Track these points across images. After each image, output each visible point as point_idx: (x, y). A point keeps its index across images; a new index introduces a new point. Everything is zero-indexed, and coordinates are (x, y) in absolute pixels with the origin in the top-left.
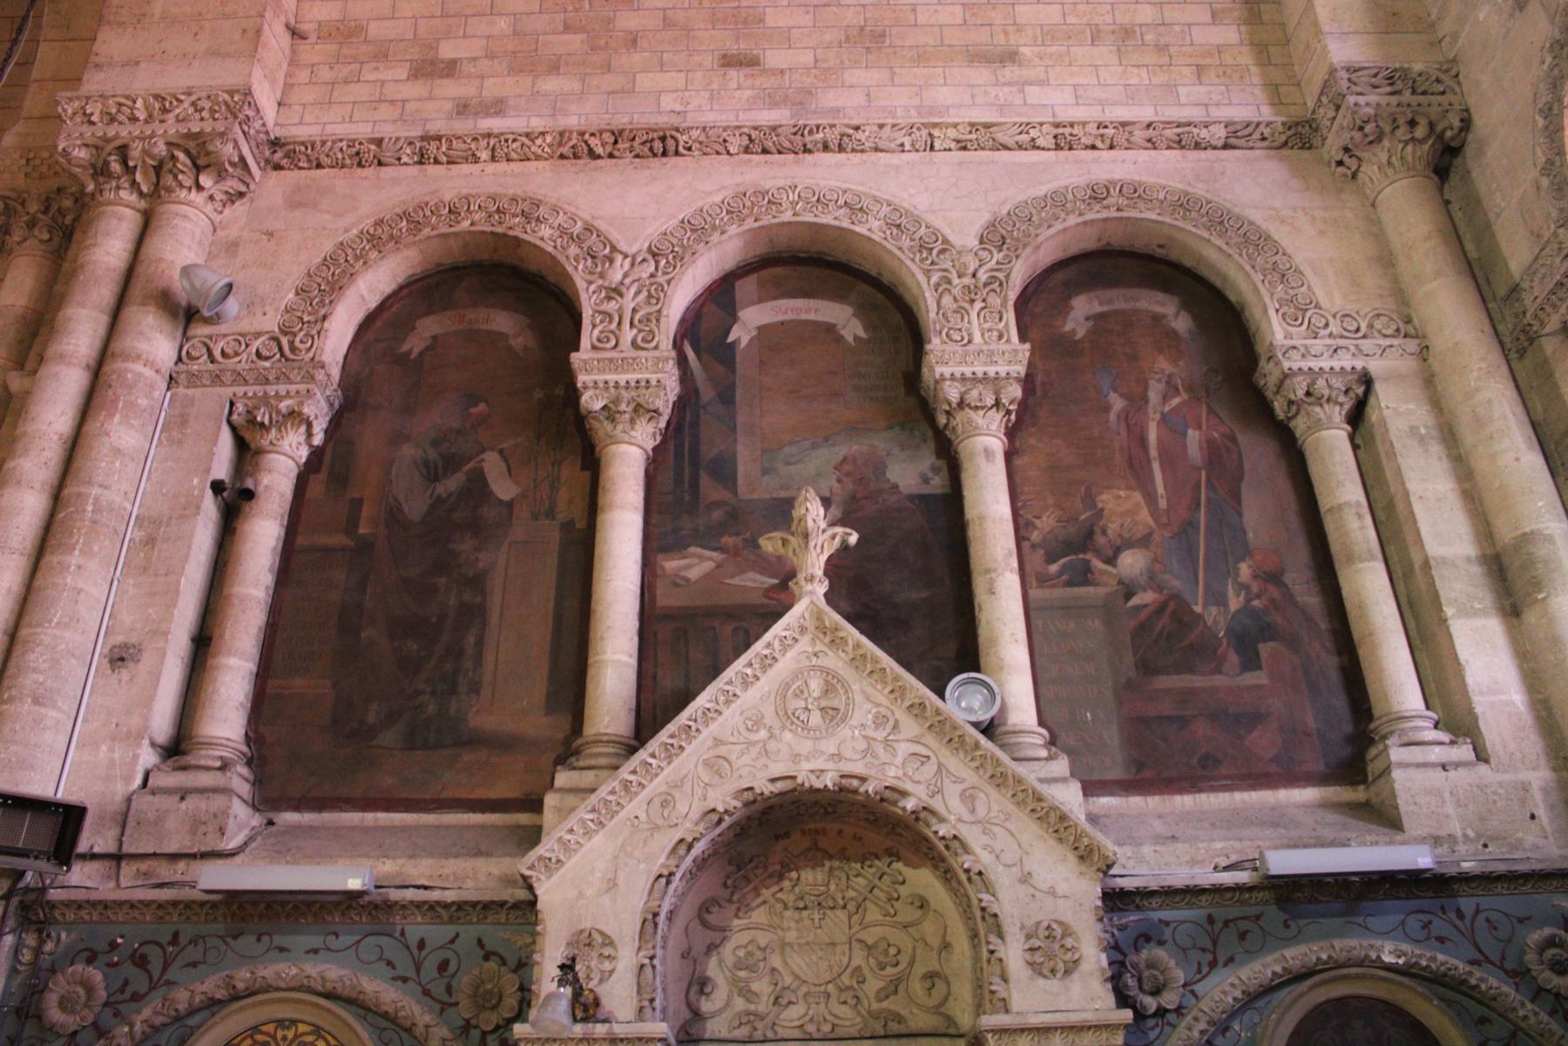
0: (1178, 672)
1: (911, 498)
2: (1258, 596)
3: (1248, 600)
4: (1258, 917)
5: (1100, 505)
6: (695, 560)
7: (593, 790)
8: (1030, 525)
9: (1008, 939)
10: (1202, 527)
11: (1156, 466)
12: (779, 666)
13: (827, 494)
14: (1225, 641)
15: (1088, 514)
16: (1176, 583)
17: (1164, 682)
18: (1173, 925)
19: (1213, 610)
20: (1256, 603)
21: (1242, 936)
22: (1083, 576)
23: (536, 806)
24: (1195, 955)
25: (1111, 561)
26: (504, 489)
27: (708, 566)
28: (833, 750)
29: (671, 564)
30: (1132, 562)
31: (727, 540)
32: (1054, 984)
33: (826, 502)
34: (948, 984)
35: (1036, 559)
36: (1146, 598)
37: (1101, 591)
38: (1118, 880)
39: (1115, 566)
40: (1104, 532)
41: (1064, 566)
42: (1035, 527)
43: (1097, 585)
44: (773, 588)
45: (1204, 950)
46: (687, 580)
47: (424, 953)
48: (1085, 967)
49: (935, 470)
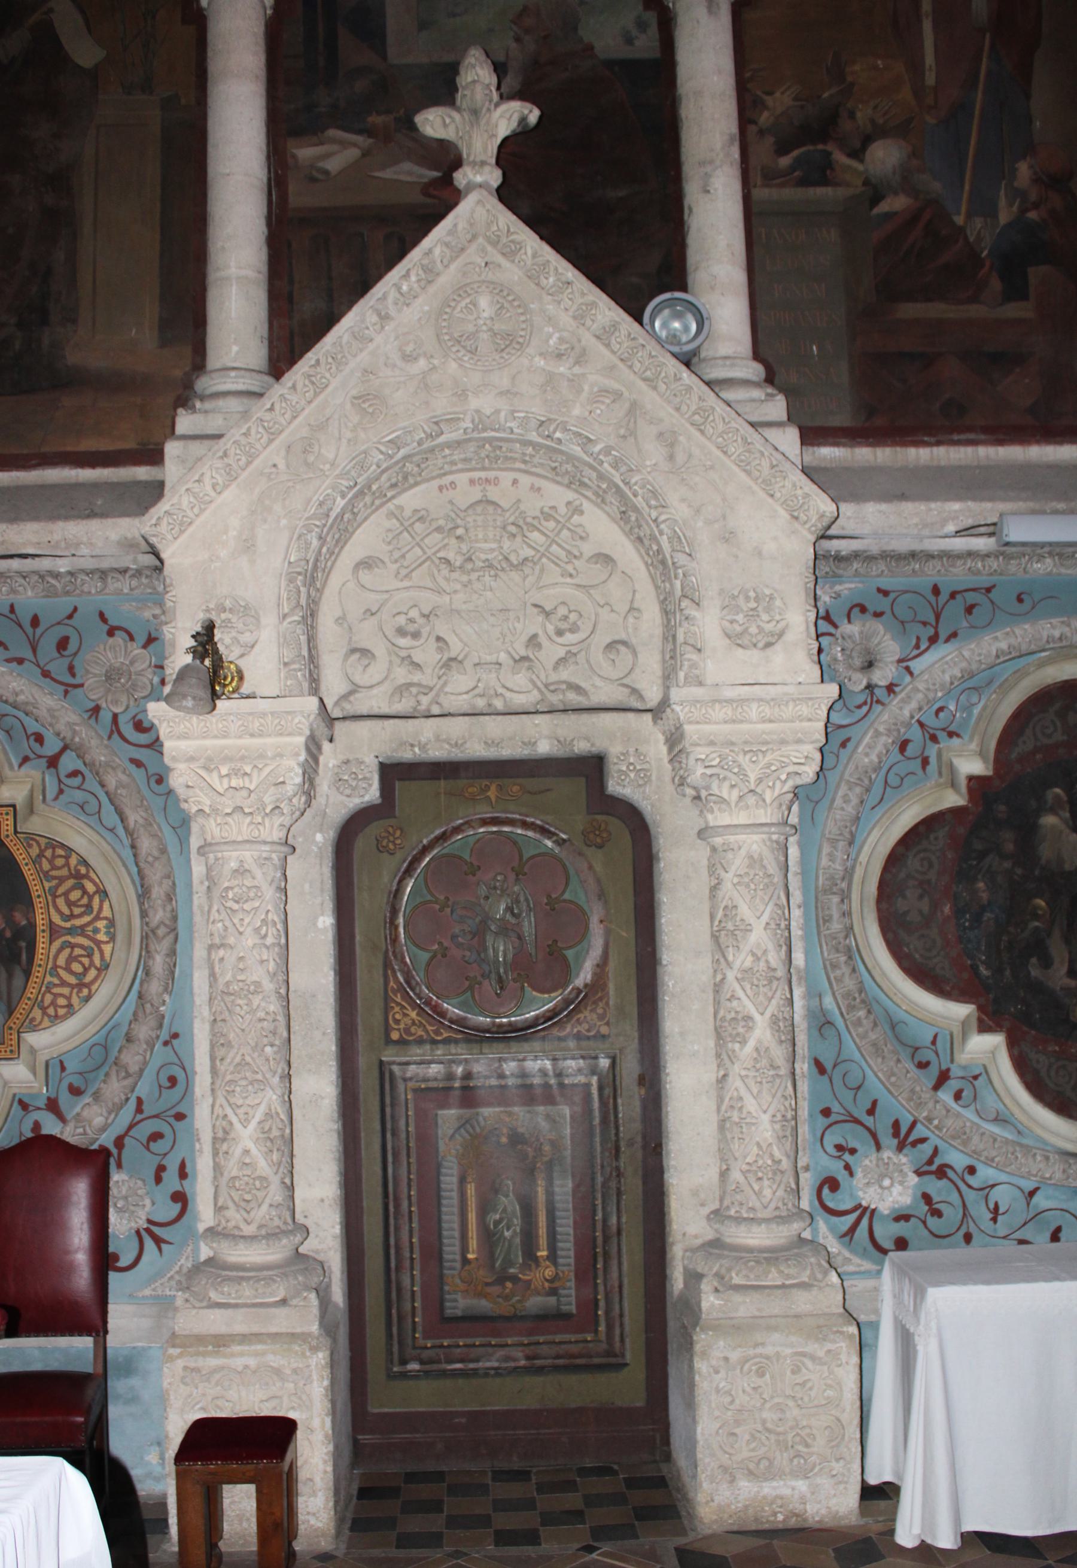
0: (928, 300)
1: (609, 64)
2: (1036, 206)
3: (1023, 211)
4: (989, 590)
5: (849, 79)
6: (335, 147)
7: (220, 436)
8: (759, 104)
9: (705, 603)
10: (977, 113)
11: (927, 26)
12: (442, 280)
13: (501, 58)
14: (988, 264)
15: (834, 90)
16: (937, 186)
17: (910, 310)
18: (892, 596)
19: (979, 222)
20: (1032, 215)
21: (969, 609)
22: (819, 173)
23: (155, 457)
24: (919, 629)
25: (858, 154)
26: (85, 53)
27: (353, 153)
28: (505, 383)
29: (305, 153)
30: (885, 157)
31: (376, 120)
32: (755, 655)
33: (500, 69)
34: (635, 653)
35: (763, 150)
36: (896, 203)
37: (841, 192)
38: (835, 542)
39: (862, 161)
40: (852, 115)
41: (798, 161)
42: (765, 107)
43: (836, 185)
44: (433, 183)
45: (925, 624)
46: (326, 172)
47: (39, 631)
48: (789, 637)
49: (642, 26)
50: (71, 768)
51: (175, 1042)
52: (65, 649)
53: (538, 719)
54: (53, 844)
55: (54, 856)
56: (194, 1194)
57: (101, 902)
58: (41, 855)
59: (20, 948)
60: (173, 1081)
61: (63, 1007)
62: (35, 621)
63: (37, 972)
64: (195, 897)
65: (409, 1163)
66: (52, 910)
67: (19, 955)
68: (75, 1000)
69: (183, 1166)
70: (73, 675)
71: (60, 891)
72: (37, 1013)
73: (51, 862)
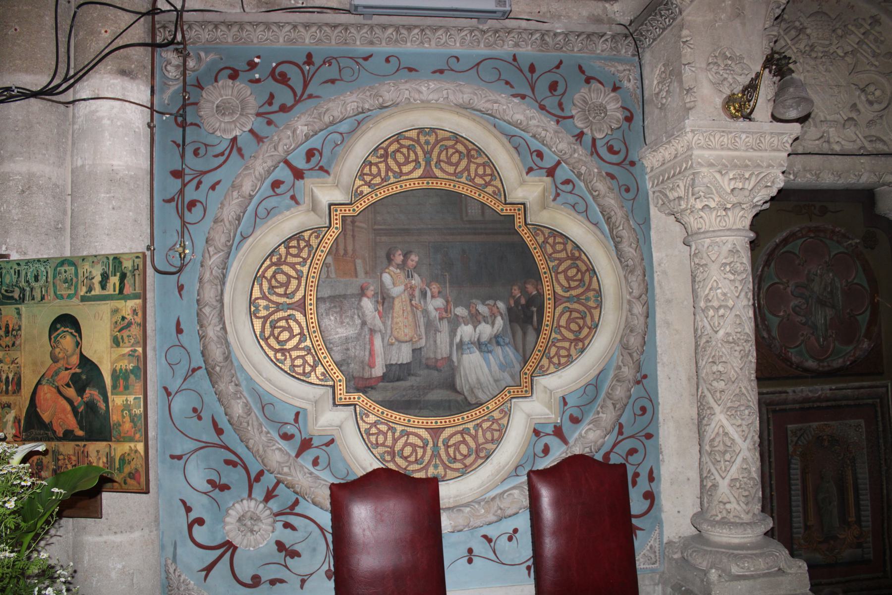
47: (535, 76)
50: (565, 178)
51: (644, 381)
52: (555, 90)
53: (863, 160)
54: (555, 233)
55: (555, 243)
56: (659, 492)
57: (591, 278)
58: (545, 242)
59: (533, 312)
60: (644, 410)
61: (563, 357)
62: (532, 69)
63: (546, 330)
64: (655, 275)
65: (770, 462)
66: (304, 324)
67: (532, 317)
68: (573, 352)
69: (651, 472)
70: (562, 110)
71: (561, 269)
72: (545, 362)
73: (553, 247)
